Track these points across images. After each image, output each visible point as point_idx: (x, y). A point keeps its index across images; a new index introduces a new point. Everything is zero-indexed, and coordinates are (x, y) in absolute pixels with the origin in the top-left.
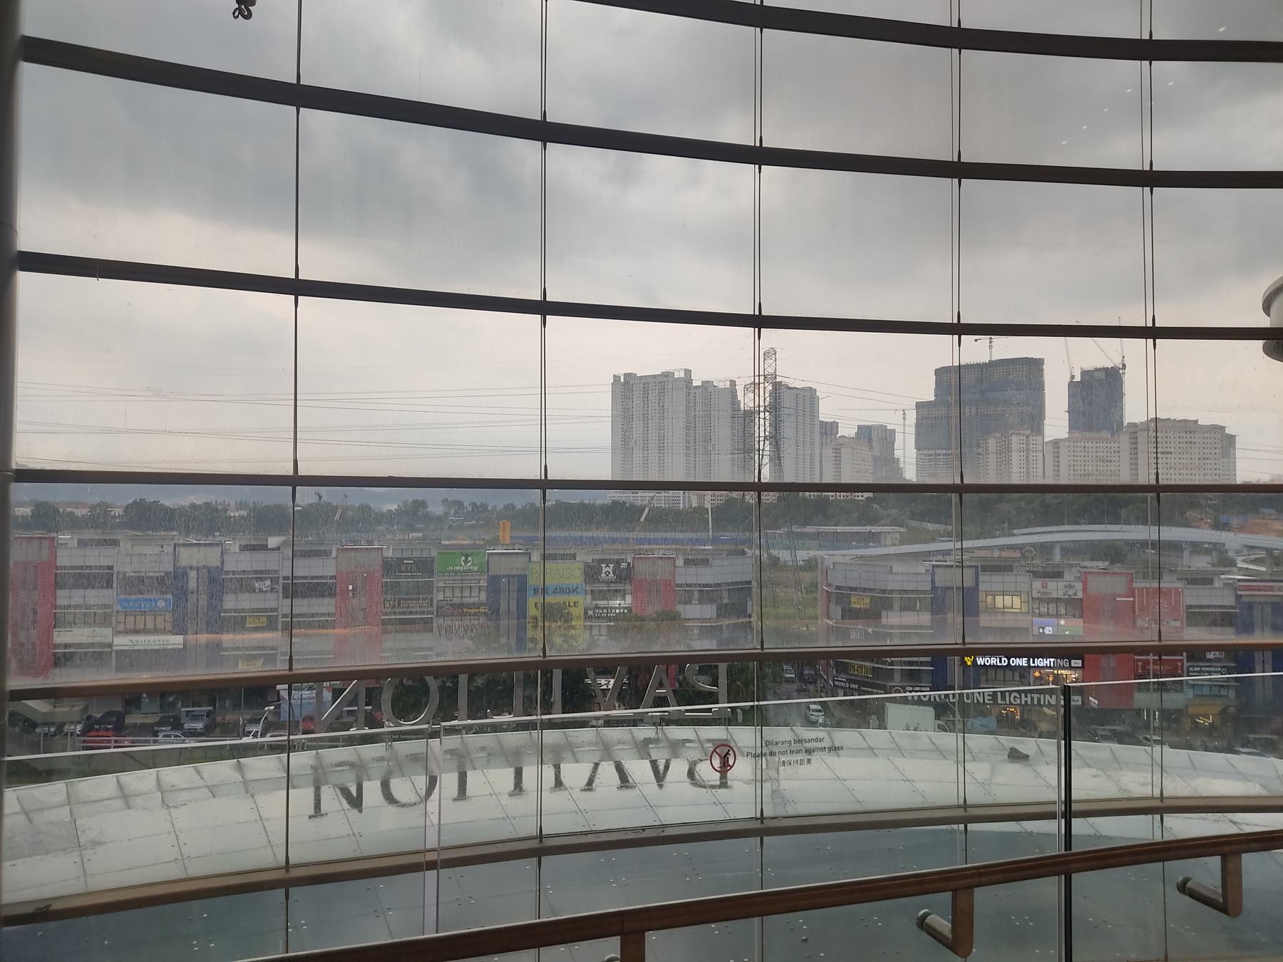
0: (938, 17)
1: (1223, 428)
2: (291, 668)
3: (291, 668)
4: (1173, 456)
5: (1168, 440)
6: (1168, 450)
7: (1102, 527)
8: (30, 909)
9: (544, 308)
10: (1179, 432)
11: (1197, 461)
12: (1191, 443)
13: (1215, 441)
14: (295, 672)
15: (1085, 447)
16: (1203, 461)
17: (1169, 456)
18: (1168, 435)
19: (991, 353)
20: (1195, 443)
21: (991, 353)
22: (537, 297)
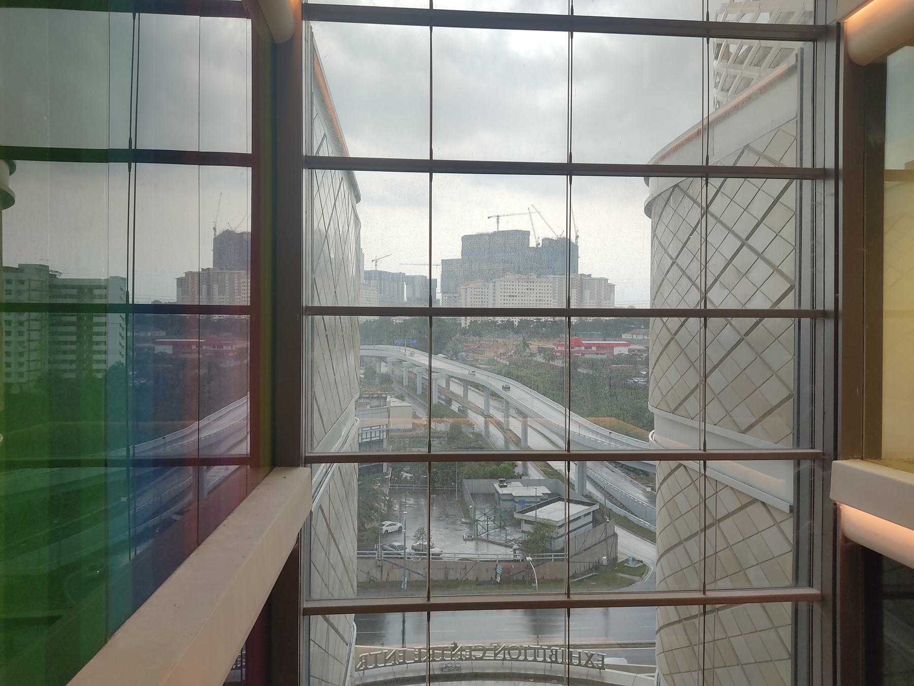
0: (558, 9)
1: (606, 280)
2: (429, 451)
3: (429, 451)
4: (518, 298)
5: (514, 287)
6: (514, 294)
7: (371, 347)
8: (794, 615)
9: (432, 166)
10: (548, 283)
11: (535, 302)
12: (531, 289)
13: (548, 288)
14: (432, 453)
15: (482, 292)
16: (539, 302)
17: (514, 298)
18: (515, 284)
19: (498, 226)
20: (527, 289)
21: (498, 226)
22: (564, 160)
